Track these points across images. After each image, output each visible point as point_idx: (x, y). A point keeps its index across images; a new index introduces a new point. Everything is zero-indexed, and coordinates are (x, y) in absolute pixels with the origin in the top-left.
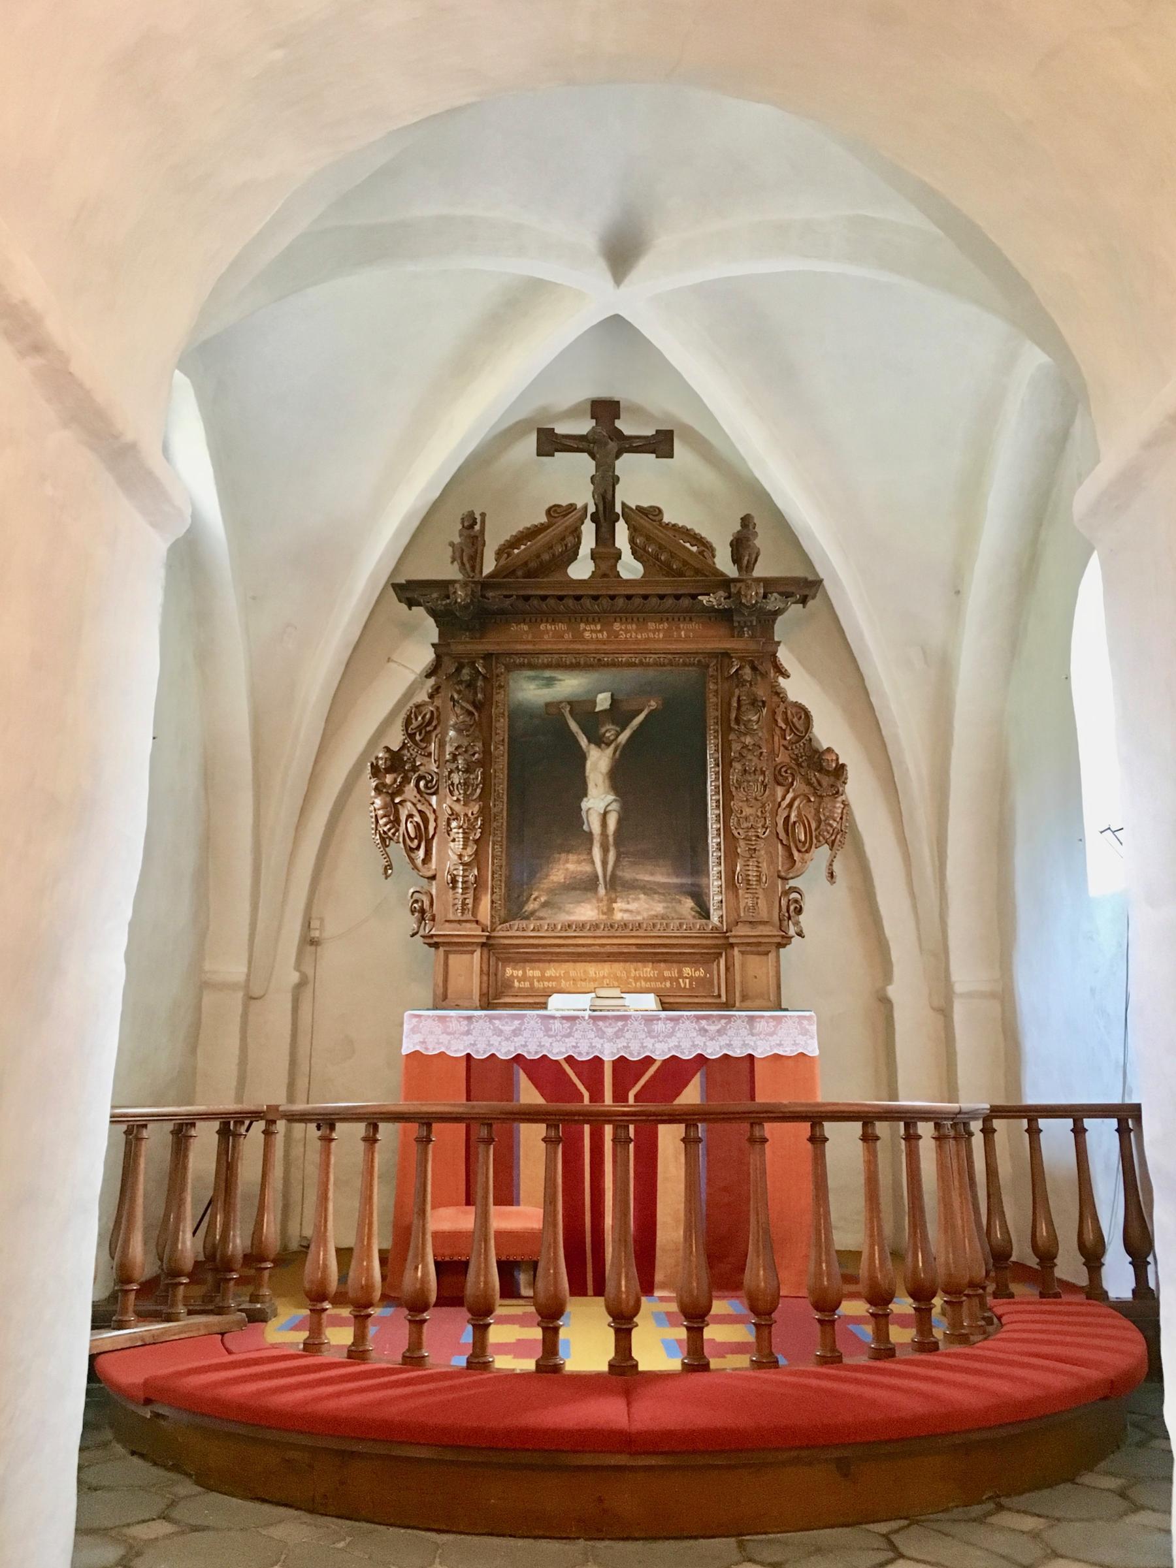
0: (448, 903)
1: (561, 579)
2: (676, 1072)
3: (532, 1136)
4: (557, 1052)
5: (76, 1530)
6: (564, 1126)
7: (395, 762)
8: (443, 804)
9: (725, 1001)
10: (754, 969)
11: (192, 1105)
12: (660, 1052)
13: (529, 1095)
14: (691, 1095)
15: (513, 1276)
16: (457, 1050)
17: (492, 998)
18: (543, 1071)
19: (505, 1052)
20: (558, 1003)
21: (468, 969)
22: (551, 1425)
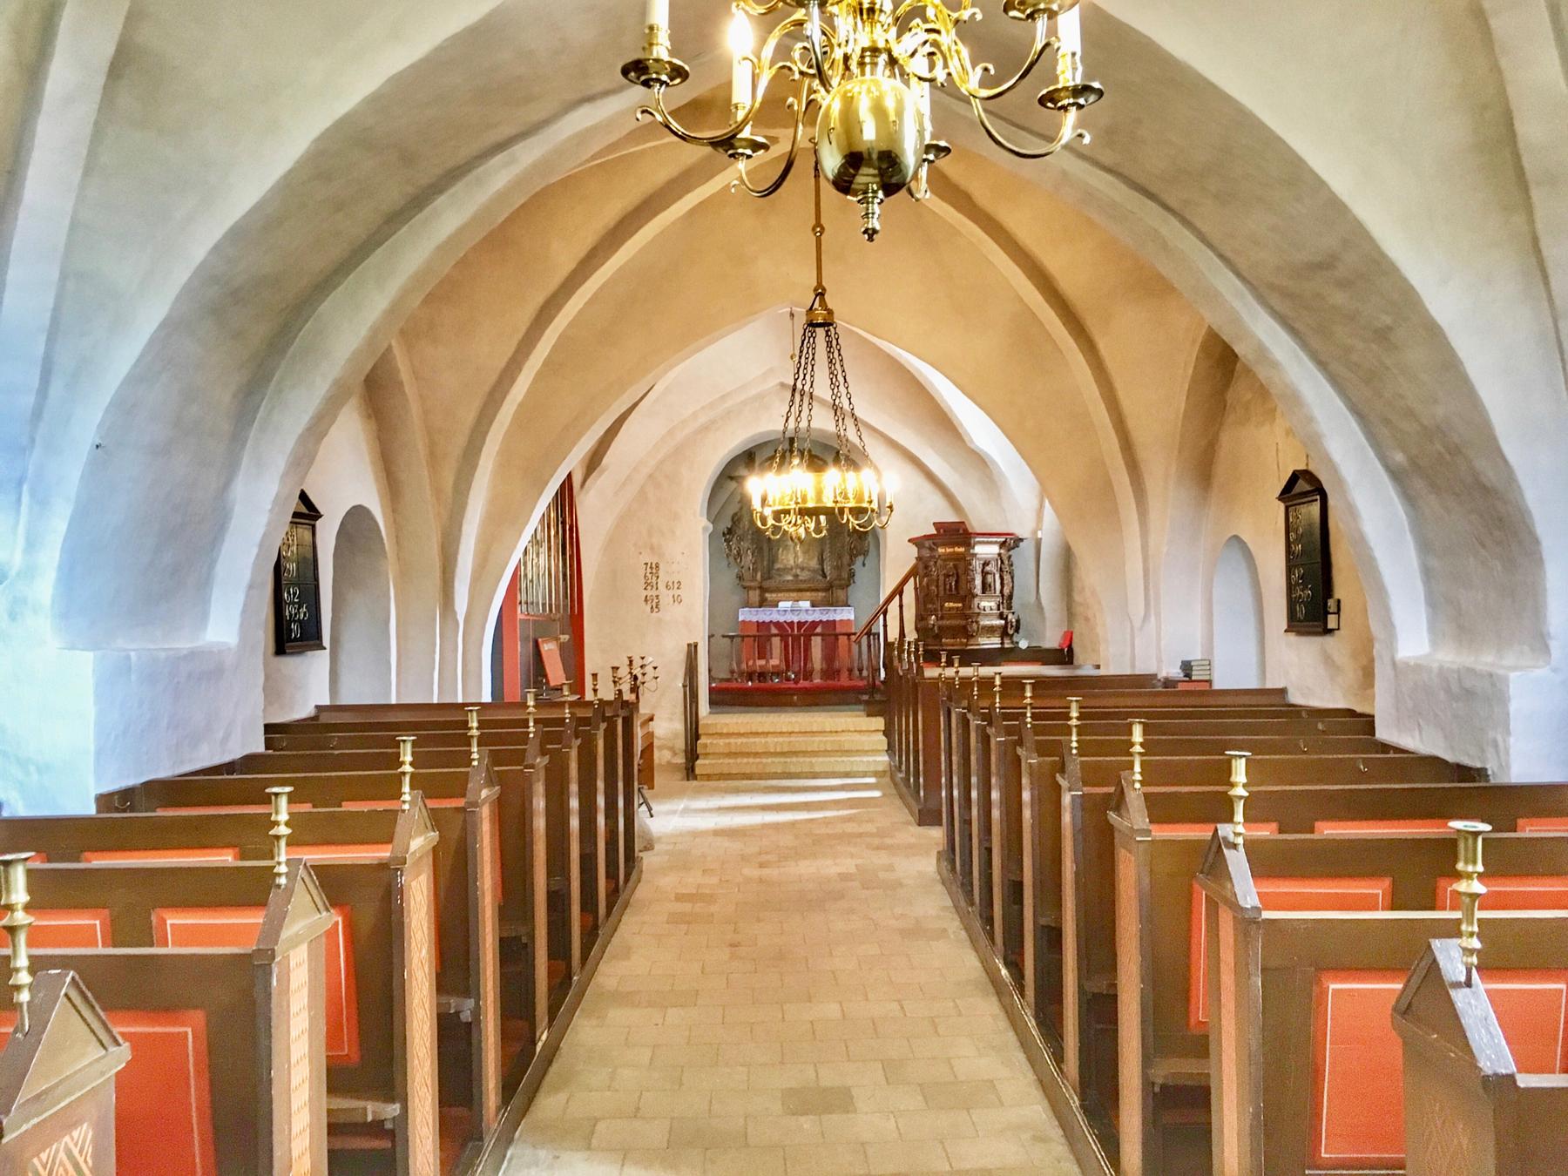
0: (747, 575)
1: (962, 112)
2: (814, 624)
3: (776, 641)
4: (782, 619)
5: (329, 1125)
6: (784, 638)
7: (730, 531)
8: (744, 545)
9: (832, 603)
10: (840, 594)
11: (1432, 908)
12: (810, 619)
13: (774, 631)
14: (819, 630)
15: (1267, 820)
16: (754, 619)
17: (762, 603)
18: (778, 624)
19: (767, 619)
20: (781, 604)
21: (754, 596)
22: (470, 501)
